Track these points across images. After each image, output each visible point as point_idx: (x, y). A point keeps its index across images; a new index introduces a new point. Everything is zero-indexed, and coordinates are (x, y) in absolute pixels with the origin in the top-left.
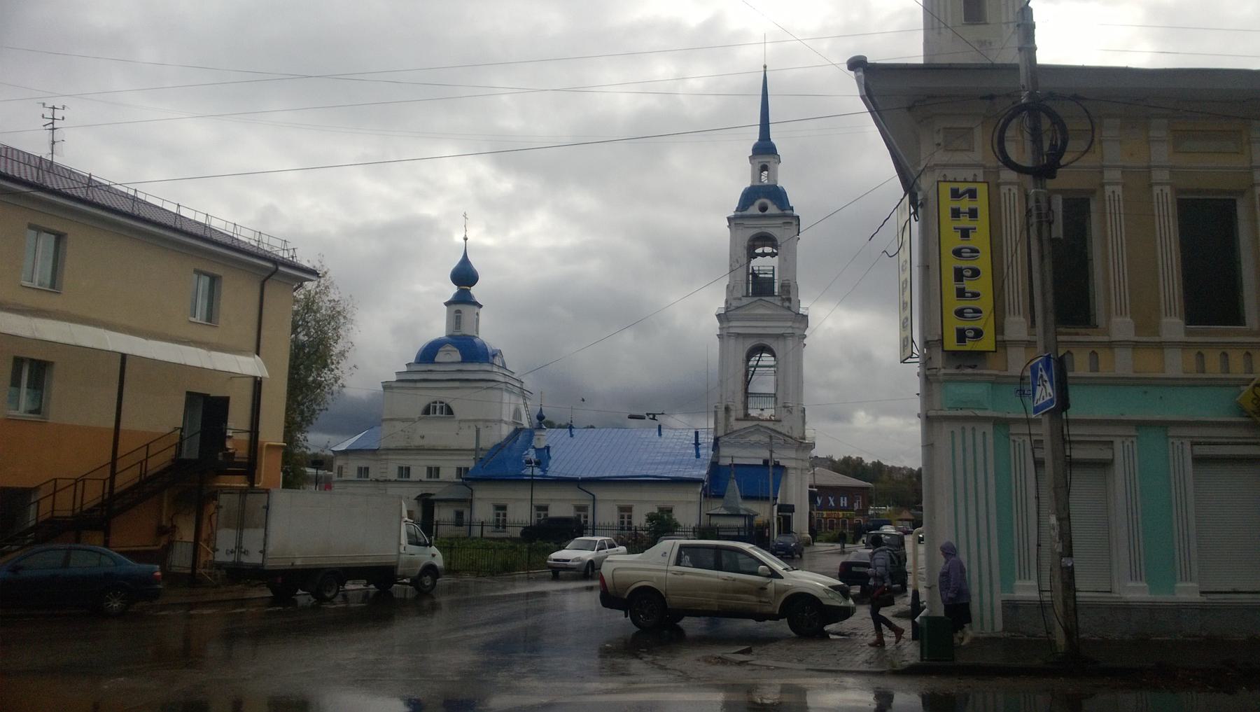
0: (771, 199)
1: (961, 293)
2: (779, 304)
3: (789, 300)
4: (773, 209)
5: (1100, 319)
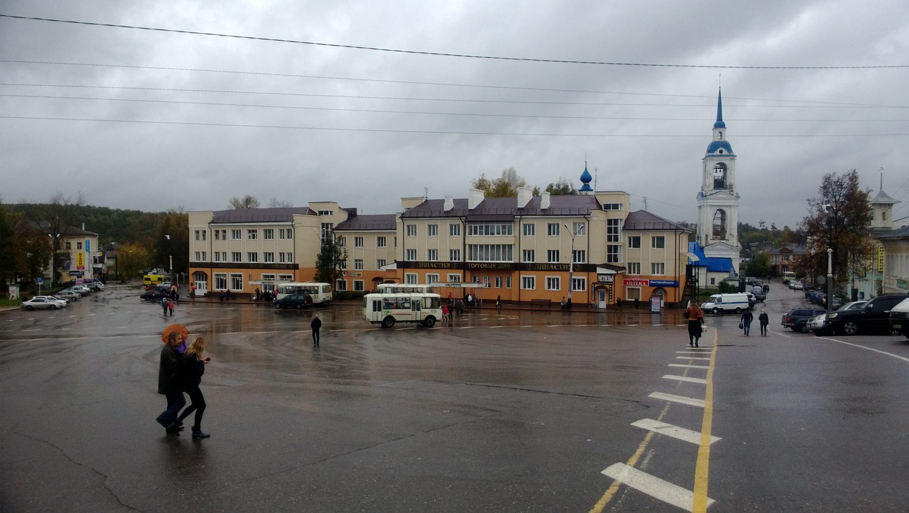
0: (724, 148)
1: (881, 263)
4: (725, 152)
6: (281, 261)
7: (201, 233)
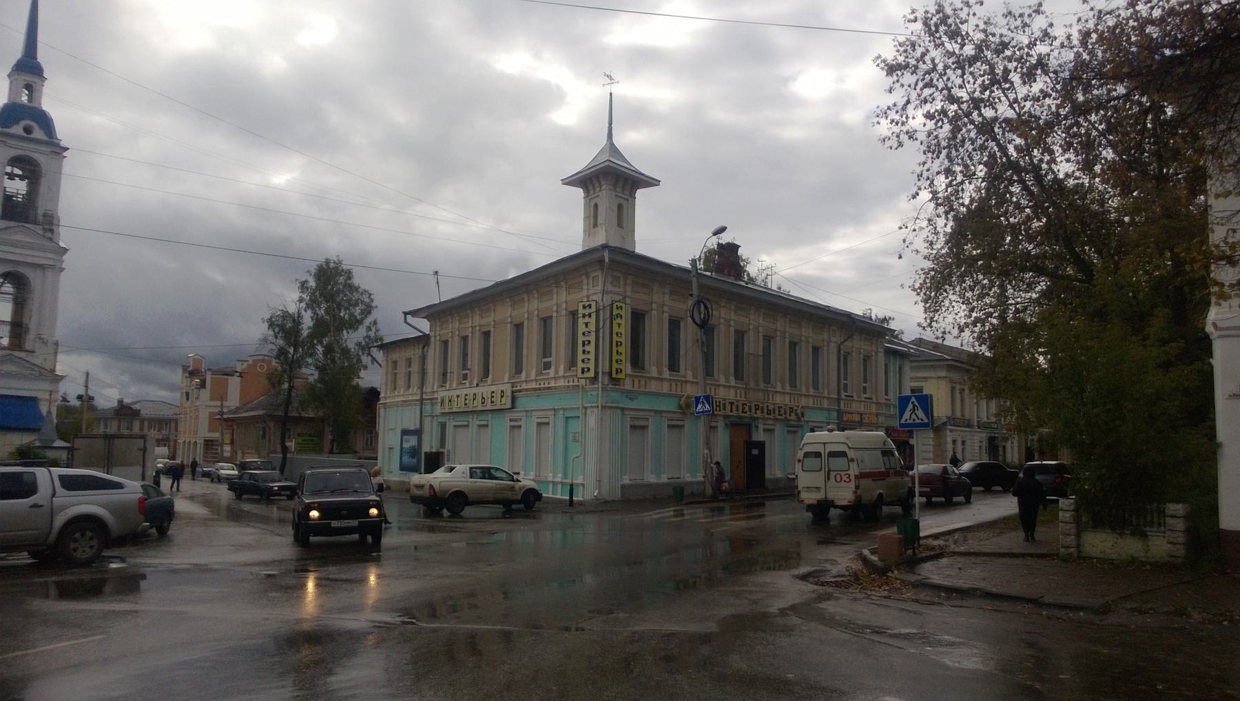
1: (584, 352)
2: (40, 232)
3: (52, 231)
4: (38, 134)
5: (647, 366)
6: (814, 404)
7: (513, 424)
